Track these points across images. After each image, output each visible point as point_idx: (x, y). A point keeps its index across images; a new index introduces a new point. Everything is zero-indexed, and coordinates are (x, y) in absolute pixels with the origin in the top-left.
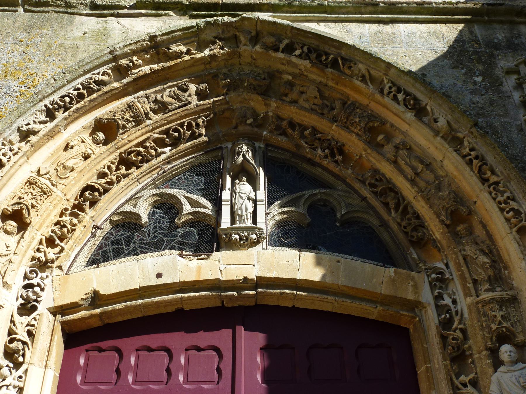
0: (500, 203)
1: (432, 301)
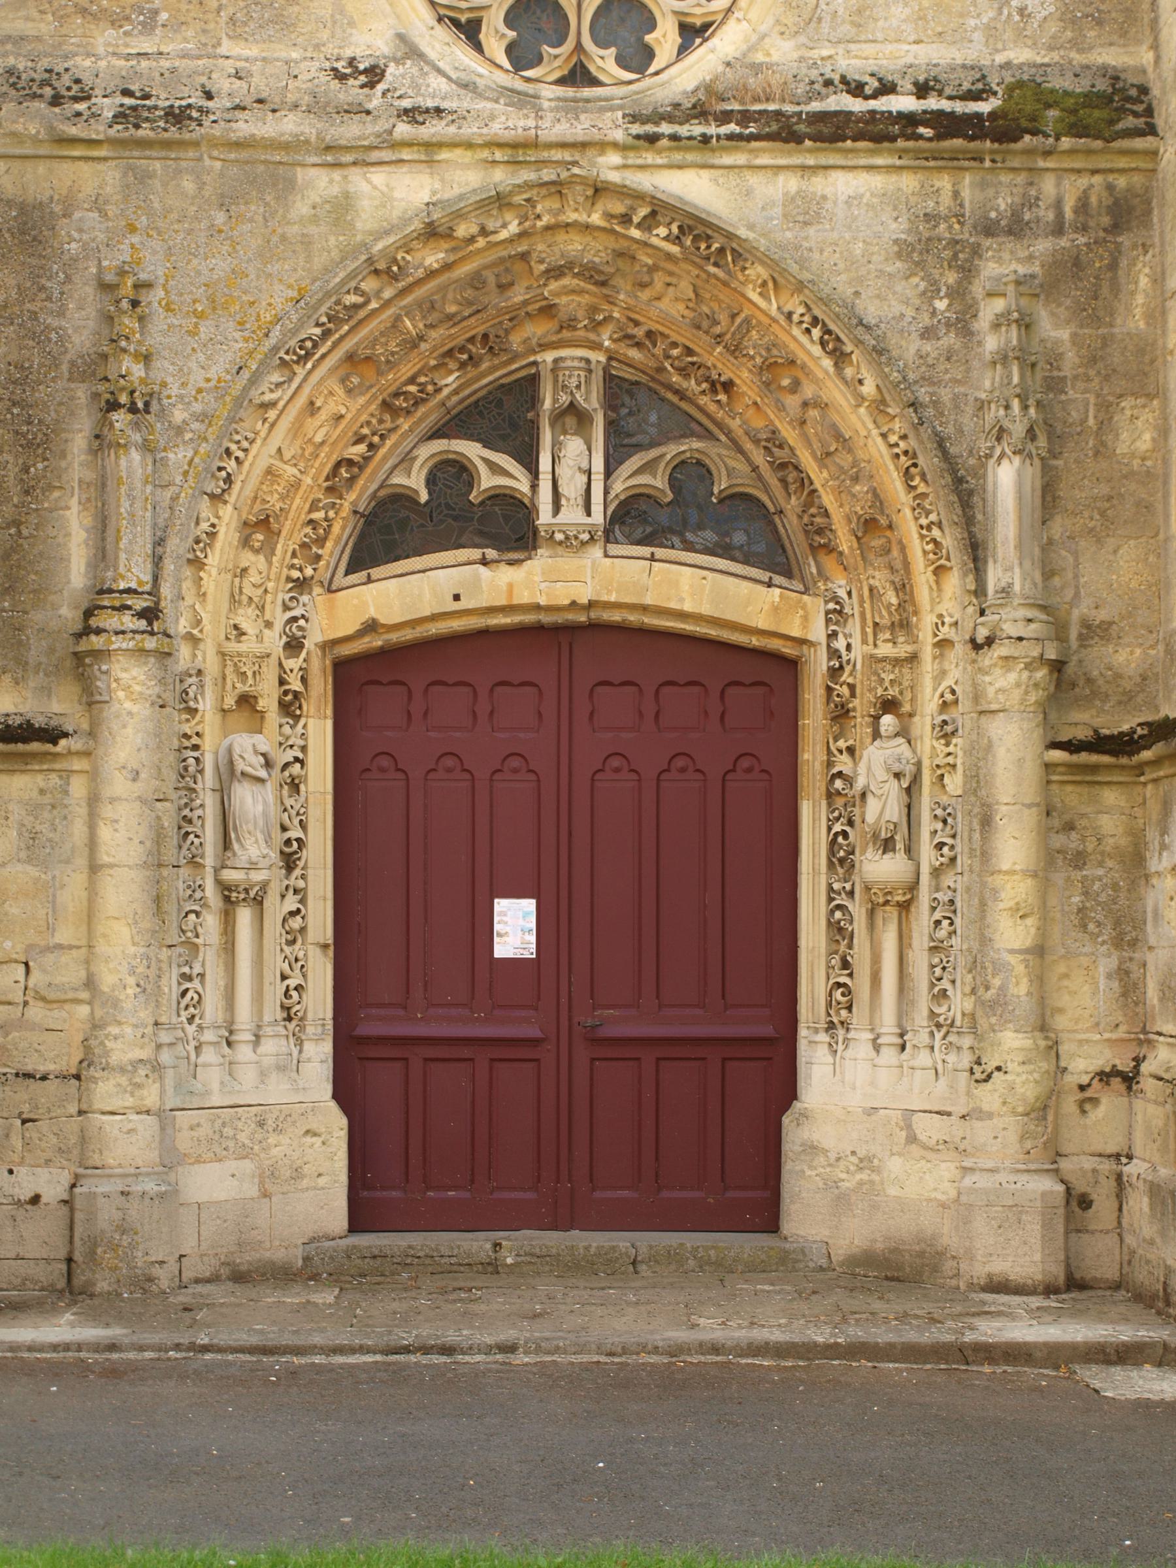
0: (922, 527)
1: (824, 640)
